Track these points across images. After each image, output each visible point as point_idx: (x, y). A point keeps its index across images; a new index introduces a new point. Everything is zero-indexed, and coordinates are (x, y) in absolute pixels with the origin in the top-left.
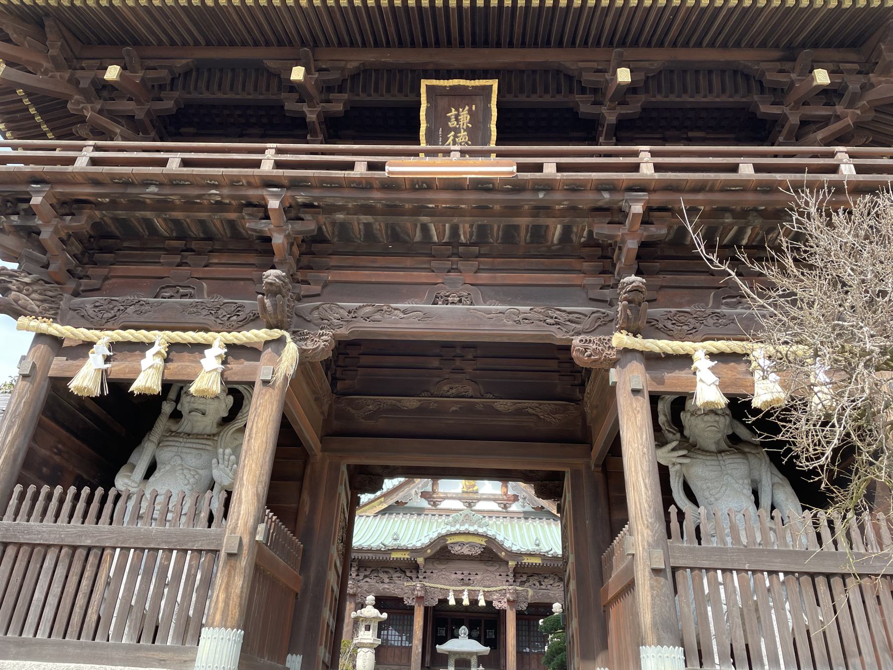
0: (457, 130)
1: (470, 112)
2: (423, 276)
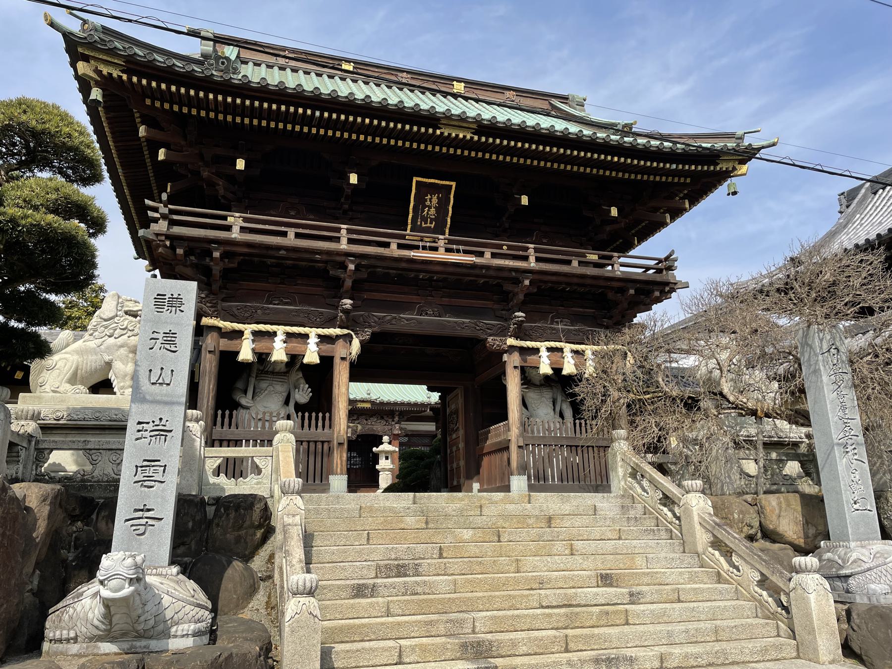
0: (430, 207)
1: (438, 197)
2: (414, 298)
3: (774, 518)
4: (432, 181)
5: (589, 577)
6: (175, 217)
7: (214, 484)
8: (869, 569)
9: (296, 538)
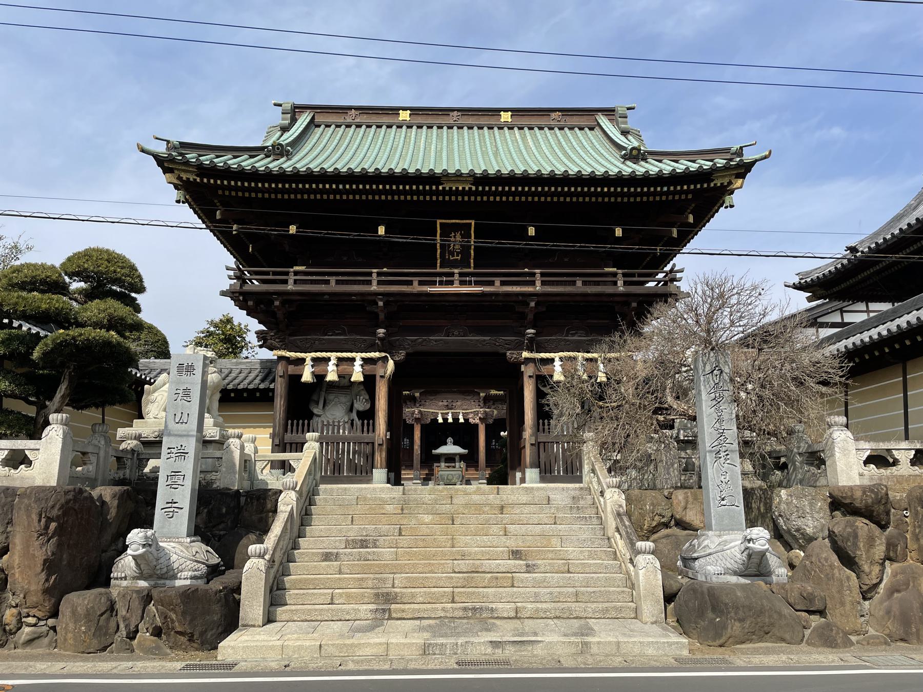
3: (680, 509)
4: (454, 221)
5: (502, 552)
8: (710, 554)
9: (281, 520)
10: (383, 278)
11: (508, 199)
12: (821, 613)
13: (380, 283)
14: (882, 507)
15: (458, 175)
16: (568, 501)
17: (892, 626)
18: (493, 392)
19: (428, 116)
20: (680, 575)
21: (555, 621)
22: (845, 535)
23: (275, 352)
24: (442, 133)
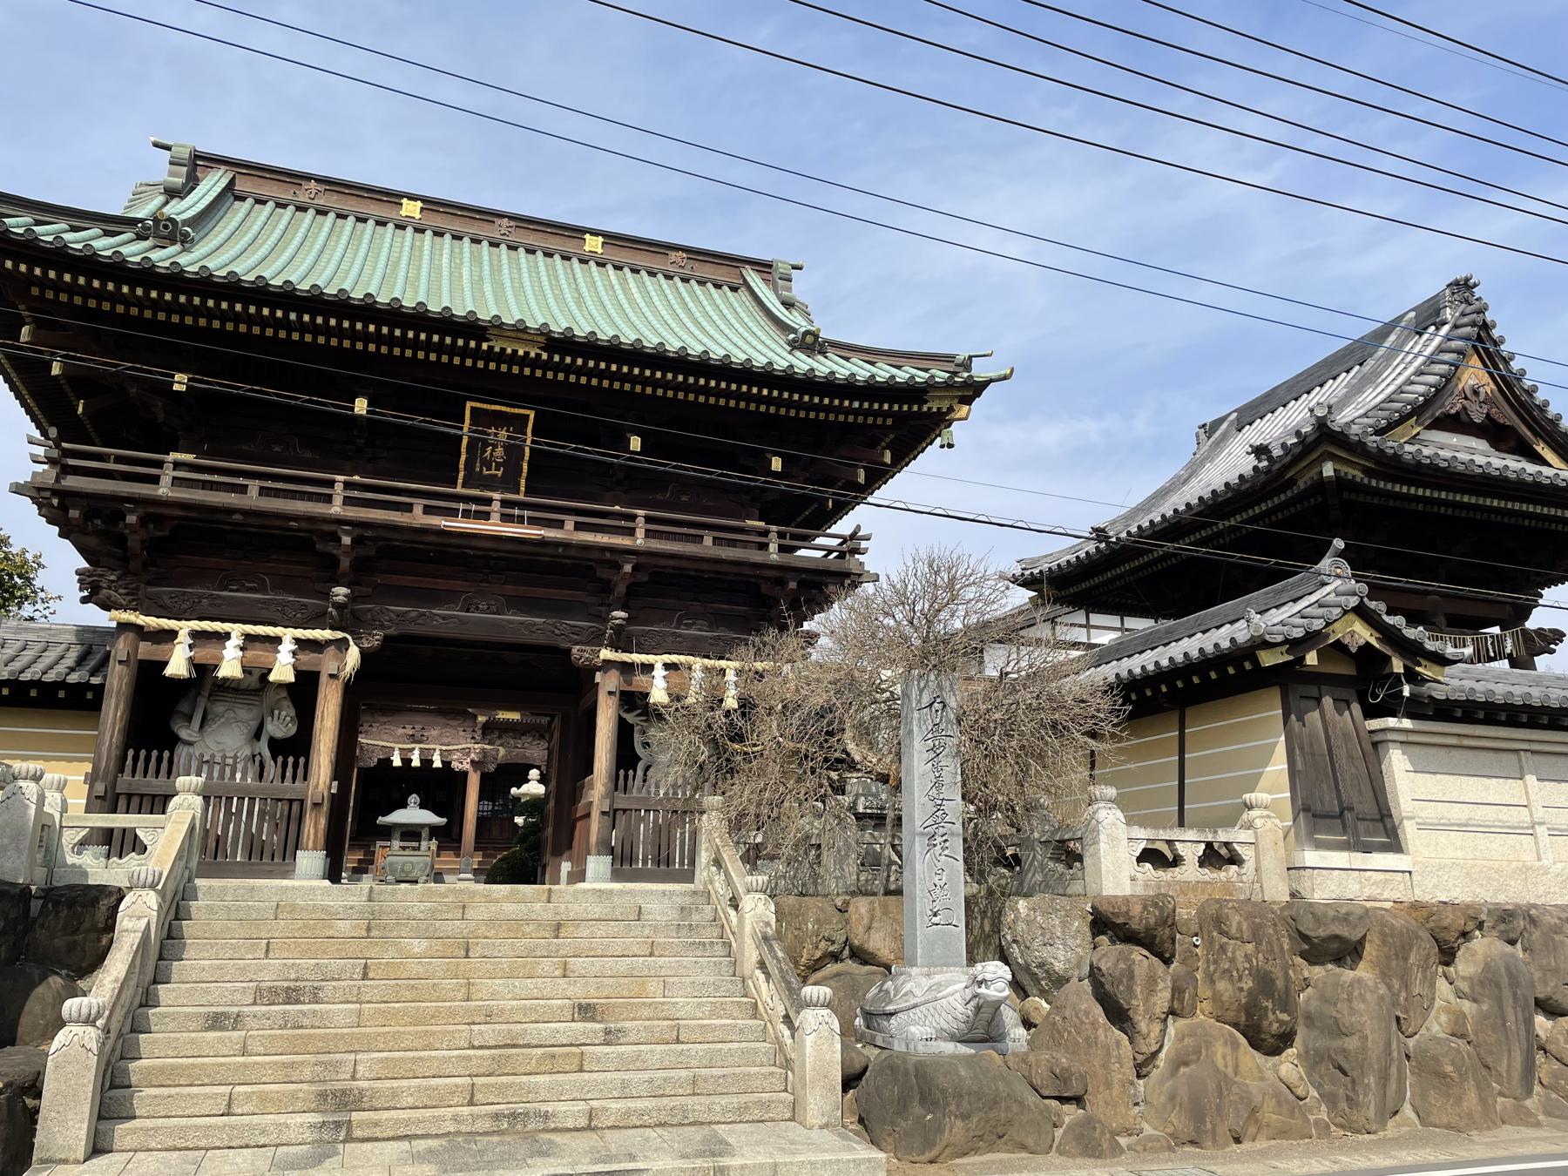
0: (495, 446)
2: (459, 585)
3: (861, 930)
5: (561, 1008)
6: (71, 462)
7: (74, 865)
10: (356, 494)
11: (589, 381)
12: (1078, 1100)
13: (348, 501)
14: (1167, 931)
15: (520, 330)
16: (673, 915)
17: (1178, 1120)
18: (503, 715)
19: (452, 217)
20: (858, 1041)
21: (659, 1130)
22: (1117, 973)
23: (114, 613)
24: (383, 236)
